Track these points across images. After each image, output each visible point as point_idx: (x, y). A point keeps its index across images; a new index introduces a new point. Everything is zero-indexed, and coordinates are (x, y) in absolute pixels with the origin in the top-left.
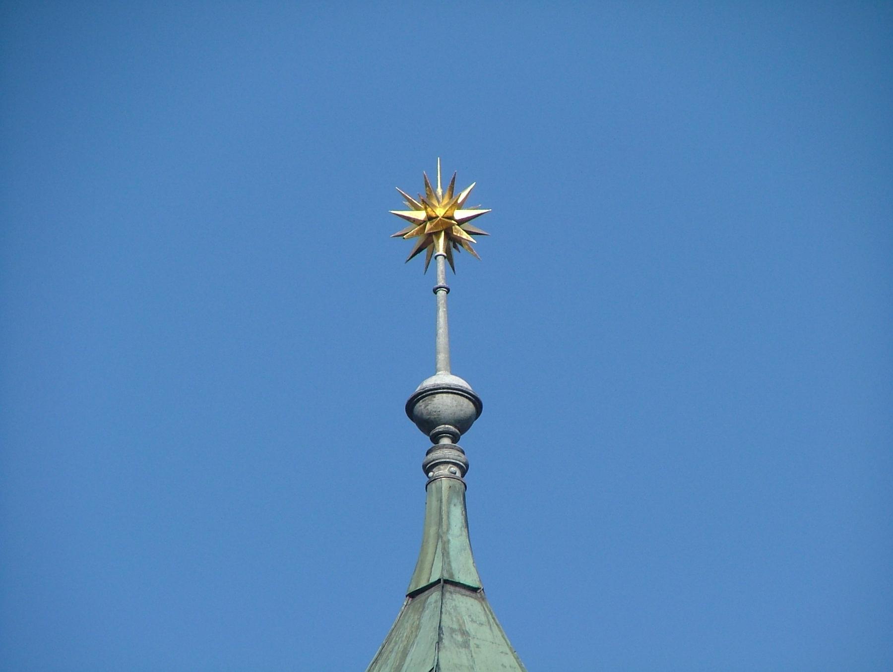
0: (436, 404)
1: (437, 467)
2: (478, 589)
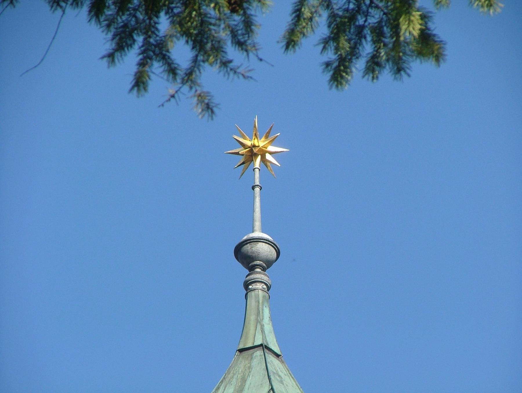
0: (258, 248)
1: (255, 283)
2: (280, 356)
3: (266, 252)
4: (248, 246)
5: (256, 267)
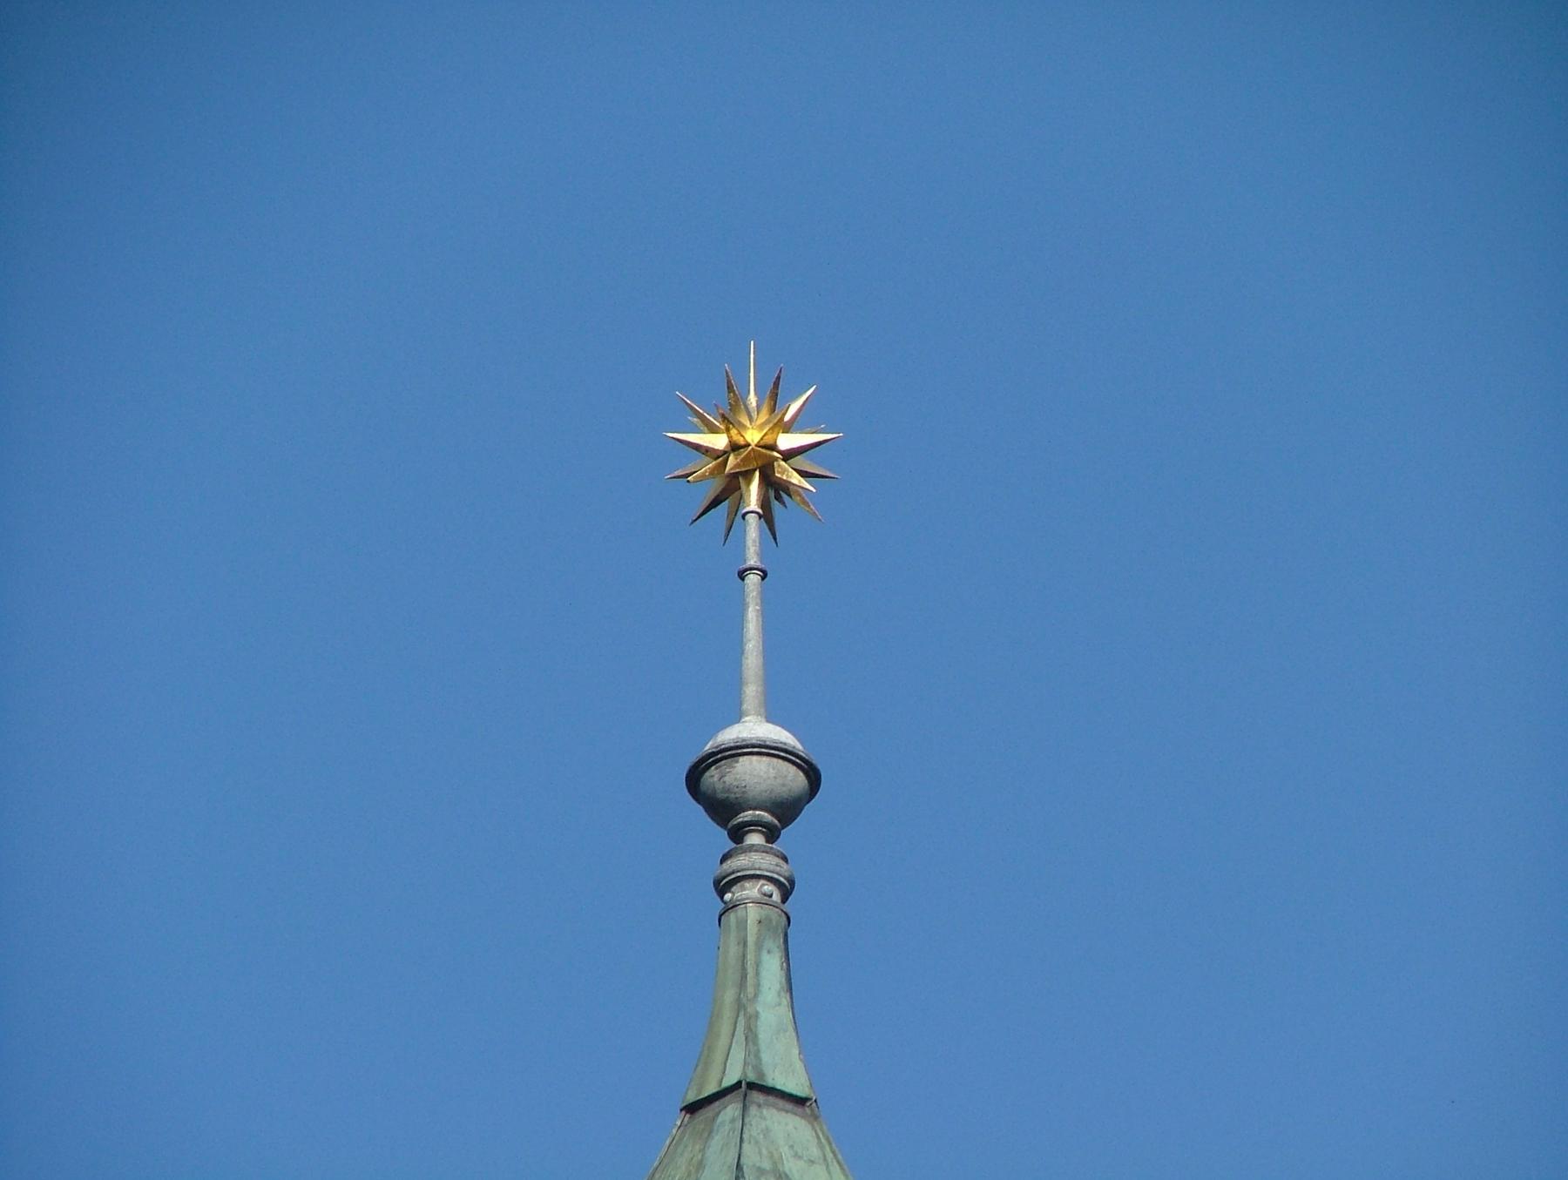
1: (739, 884)
3: (764, 780)
4: (713, 774)
5: (747, 829)
